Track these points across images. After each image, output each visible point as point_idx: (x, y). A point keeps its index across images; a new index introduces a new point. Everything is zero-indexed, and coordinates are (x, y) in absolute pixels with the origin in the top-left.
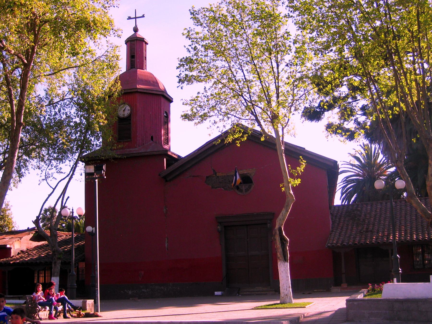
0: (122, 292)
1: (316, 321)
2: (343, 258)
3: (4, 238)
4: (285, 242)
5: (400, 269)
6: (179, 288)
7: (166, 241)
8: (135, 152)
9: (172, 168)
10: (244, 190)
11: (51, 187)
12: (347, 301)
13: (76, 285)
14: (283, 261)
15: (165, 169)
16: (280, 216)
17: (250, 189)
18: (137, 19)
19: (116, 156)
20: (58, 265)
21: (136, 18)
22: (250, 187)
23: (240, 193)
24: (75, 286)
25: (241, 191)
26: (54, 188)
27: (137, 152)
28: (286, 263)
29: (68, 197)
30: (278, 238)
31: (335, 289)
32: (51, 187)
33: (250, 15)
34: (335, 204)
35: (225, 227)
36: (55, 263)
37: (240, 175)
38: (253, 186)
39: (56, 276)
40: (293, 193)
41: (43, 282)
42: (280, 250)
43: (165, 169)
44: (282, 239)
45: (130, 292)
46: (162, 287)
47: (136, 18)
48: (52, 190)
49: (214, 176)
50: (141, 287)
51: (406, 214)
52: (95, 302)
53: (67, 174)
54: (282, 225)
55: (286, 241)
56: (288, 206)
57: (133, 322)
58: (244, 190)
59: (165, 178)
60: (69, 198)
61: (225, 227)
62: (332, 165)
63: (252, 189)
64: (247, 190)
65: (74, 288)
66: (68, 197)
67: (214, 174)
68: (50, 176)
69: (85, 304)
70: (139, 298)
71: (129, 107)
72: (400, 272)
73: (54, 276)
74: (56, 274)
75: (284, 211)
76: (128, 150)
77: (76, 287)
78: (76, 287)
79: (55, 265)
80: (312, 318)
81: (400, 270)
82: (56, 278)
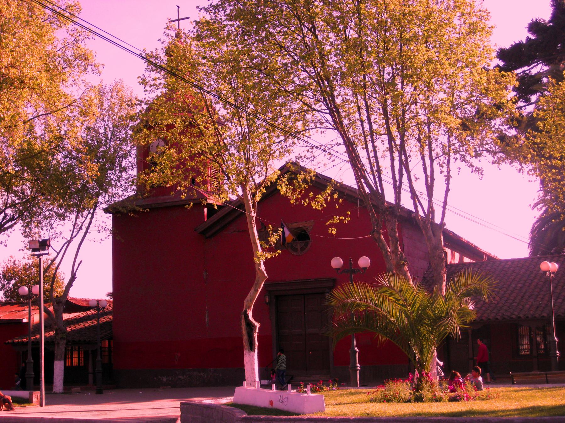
1: (439, 421)
3: (25, 310)
4: (253, 328)
7: (207, 315)
8: (169, 201)
10: (299, 249)
11: (55, 250)
12: (181, 403)
13: (33, 373)
14: (249, 350)
15: (206, 219)
17: (306, 247)
21: (178, 20)
23: (295, 253)
24: (31, 375)
26: (58, 251)
28: (252, 353)
29: (81, 262)
32: (55, 250)
33: (24, 128)
34: (64, 319)
36: (58, 344)
39: (60, 360)
43: (206, 219)
45: (165, 379)
46: (202, 374)
47: (178, 20)
48: (56, 254)
50: (177, 373)
54: (250, 307)
57: (60, 419)
58: (299, 249)
59: (203, 233)
60: (82, 263)
64: (302, 249)
66: (81, 262)
67: (262, 229)
68: (58, 235)
71: (163, 142)
72: (558, 355)
73: (56, 360)
74: (59, 357)
76: (162, 197)
77: (34, 376)
78: (34, 376)
81: (358, 367)
82: (59, 362)
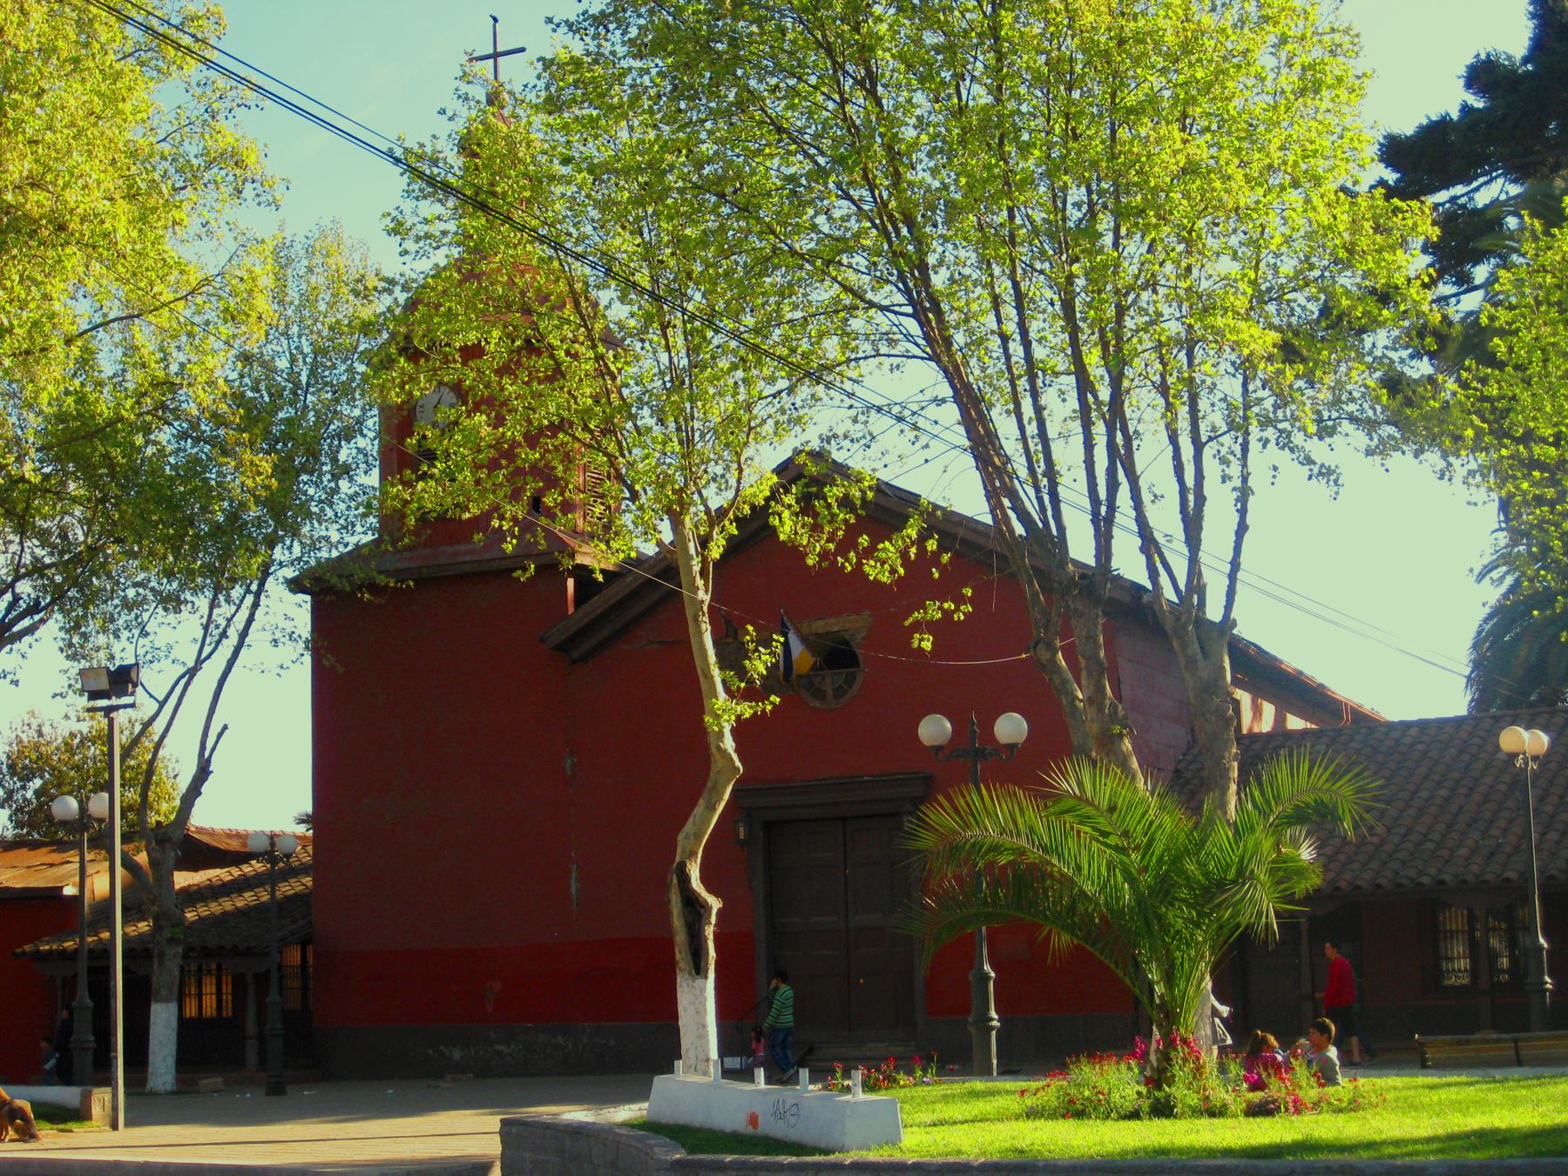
0: (431, 1052)
3: (68, 862)
4: (702, 911)
5: (1548, 979)
6: (612, 1043)
7: (574, 876)
8: (468, 558)
10: (830, 692)
11: (151, 696)
14: (690, 974)
17: (850, 687)
18: (491, 51)
20: (168, 963)
22: (850, 681)
25: (821, 695)
26: (161, 699)
27: (476, 558)
28: (699, 981)
29: (225, 727)
31: (1436, 1046)
32: (151, 696)
34: (177, 887)
35: (769, 826)
36: (162, 955)
37: (804, 640)
38: (860, 677)
39: (166, 1000)
43: (571, 610)
45: (457, 1055)
48: (156, 706)
49: (730, 640)
51: (1426, 778)
54: (693, 854)
59: (564, 647)
60: (227, 732)
61: (769, 826)
62: (1127, 599)
63: (857, 685)
64: (839, 692)
66: (225, 727)
67: (727, 636)
68: (162, 654)
72: (1548, 986)
73: (157, 1001)
74: (163, 992)
76: (449, 549)
79: (161, 963)
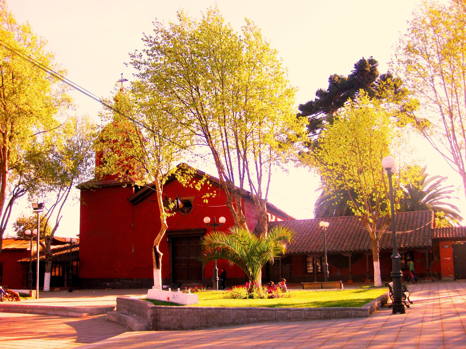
2: (350, 260)
9: (139, 193)
10: (186, 212)
16: (157, 239)
19: (95, 186)
22: (190, 209)
25: (184, 212)
28: (158, 270)
30: (154, 253)
37: (181, 201)
38: (192, 209)
39: (48, 272)
40: (167, 223)
41: (61, 275)
42: (155, 261)
44: (157, 255)
45: (108, 284)
48: (48, 211)
52: (37, 292)
53: (212, 156)
55: (160, 255)
56: (163, 231)
58: (186, 212)
59: (133, 201)
63: (192, 210)
64: (188, 212)
65: (31, 282)
69: (31, 292)
70: (113, 288)
74: (48, 271)
75: (159, 235)
76: (109, 181)
80: (418, 316)
